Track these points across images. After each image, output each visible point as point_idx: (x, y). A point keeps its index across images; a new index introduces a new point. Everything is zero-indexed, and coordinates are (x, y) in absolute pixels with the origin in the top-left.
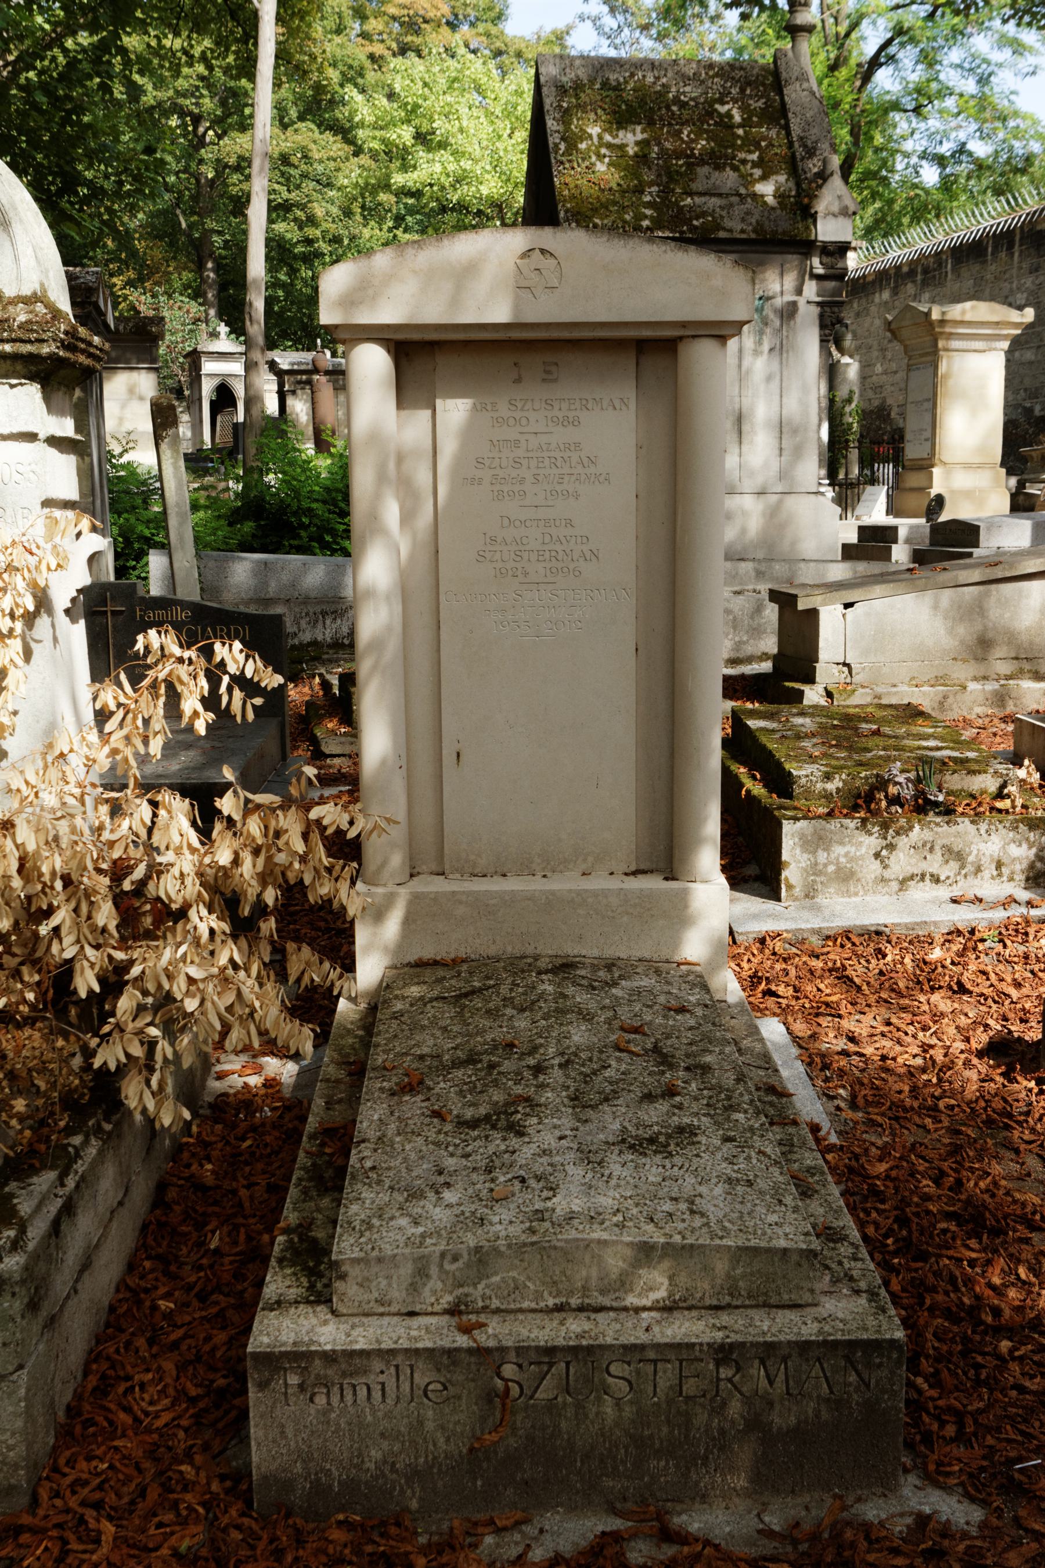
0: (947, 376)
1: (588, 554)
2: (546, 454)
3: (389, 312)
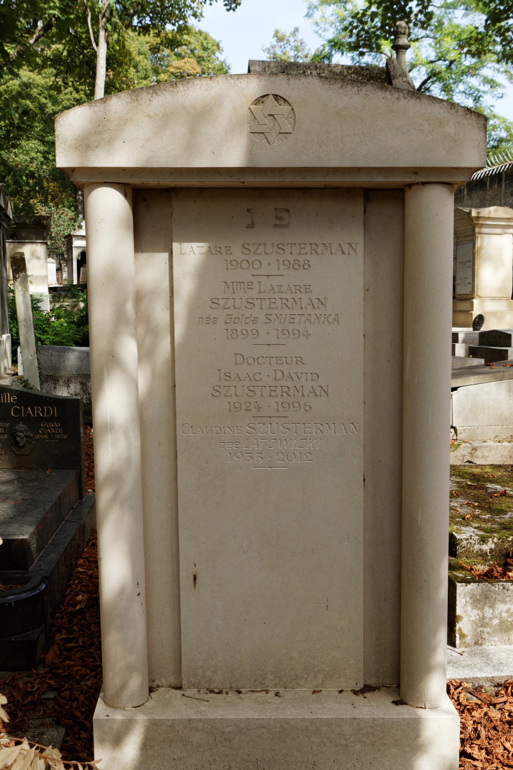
0: (481, 248)
1: (318, 390)
2: (277, 295)
3: (122, 156)
